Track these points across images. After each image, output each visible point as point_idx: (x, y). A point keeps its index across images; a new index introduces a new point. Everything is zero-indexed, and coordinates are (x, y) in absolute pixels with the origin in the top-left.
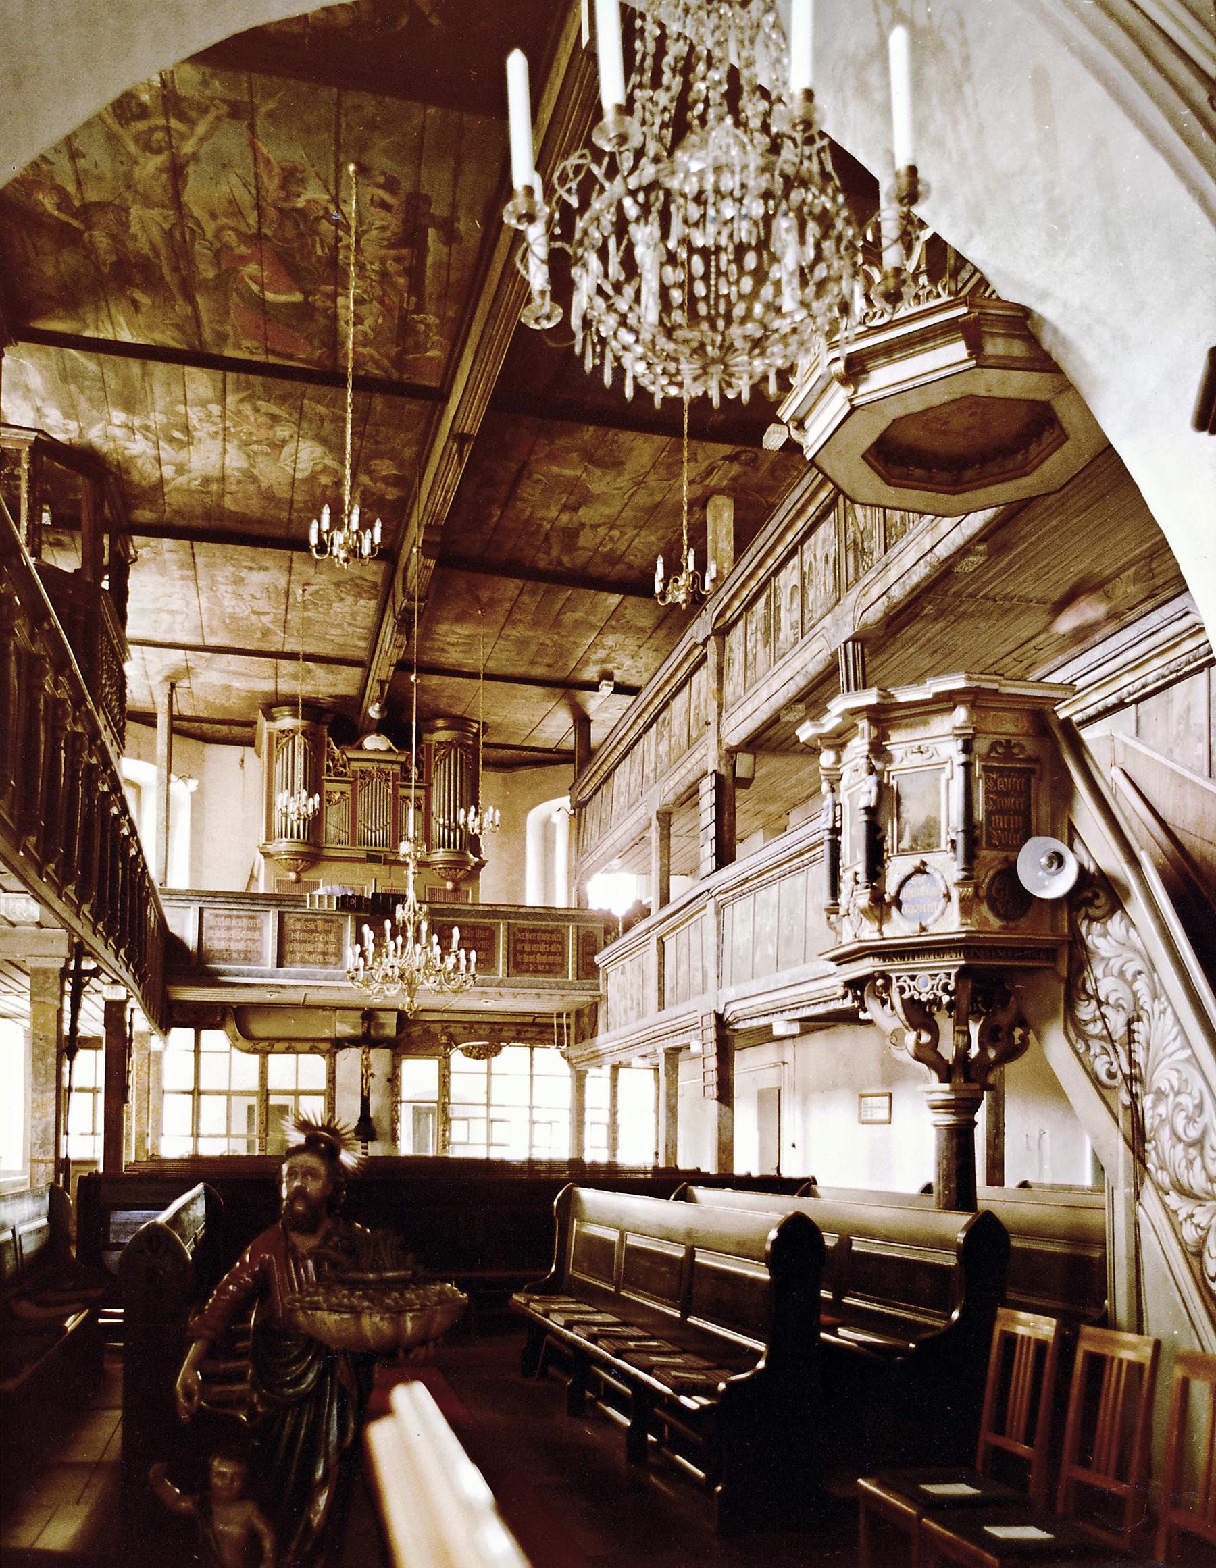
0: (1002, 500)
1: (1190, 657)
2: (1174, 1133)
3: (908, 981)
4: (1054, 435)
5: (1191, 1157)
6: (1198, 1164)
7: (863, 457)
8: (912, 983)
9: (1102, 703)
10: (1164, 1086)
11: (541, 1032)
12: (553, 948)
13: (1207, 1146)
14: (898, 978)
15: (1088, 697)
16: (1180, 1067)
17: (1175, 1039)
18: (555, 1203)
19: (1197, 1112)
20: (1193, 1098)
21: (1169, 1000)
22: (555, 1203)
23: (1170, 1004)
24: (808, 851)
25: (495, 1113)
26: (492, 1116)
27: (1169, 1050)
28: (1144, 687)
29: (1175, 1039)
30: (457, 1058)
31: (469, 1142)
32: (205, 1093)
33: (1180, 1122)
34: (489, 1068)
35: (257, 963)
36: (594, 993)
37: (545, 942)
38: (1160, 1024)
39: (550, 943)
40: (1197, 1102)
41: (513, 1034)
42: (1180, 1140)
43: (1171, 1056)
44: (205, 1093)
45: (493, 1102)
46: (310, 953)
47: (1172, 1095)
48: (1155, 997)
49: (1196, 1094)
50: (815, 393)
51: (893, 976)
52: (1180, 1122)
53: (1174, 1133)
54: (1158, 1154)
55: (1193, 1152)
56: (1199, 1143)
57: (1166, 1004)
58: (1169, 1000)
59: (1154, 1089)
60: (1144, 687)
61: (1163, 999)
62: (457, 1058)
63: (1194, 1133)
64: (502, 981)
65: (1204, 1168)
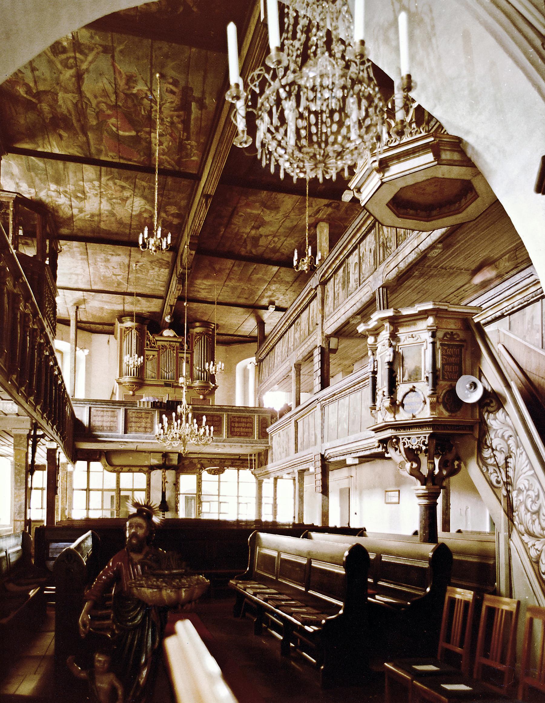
1: (534, 294)
2: (526, 508)
3: (407, 440)
5: (534, 519)
6: (537, 522)
8: (409, 441)
9: (494, 315)
10: (522, 487)
11: (243, 463)
12: (248, 425)
13: (541, 514)
14: (403, 439)
15: (488, 313)
16: (529, 478)
17: (527, 466)
18: (249, 539)
19: (537, 499)
20: (535, 492)
21: (524, 448)
22: (249, 539)
23: (525, 450)
24: (362, 382)
25: (222, 499)
26: (221, 501)
28: (513, 308)
29: (527, 466)
30: (205, 474)
31: (210, 512)
32: (92, 490)
33: (529, 503)
34: (219, 479)
35: (115, 432)
36: (266, 445)
37: (244, 422)
38: (520, 459)
42: (529, 511)
43: (525, 473)
44: (92, 490)
45: (221, 494)
46: (139, 427)
47: (525, 491)
48: (518, 447)
51: (400, 437)
52: (529, 503)
54: (519, 518)
55: (535, 516)
56: (537, 513)
57: (523, 450)
58: (524, 448)
59: (517, 488)
60: (513, 308)
61: (521, 448)
62: (205, 474)
63: (535, 508)
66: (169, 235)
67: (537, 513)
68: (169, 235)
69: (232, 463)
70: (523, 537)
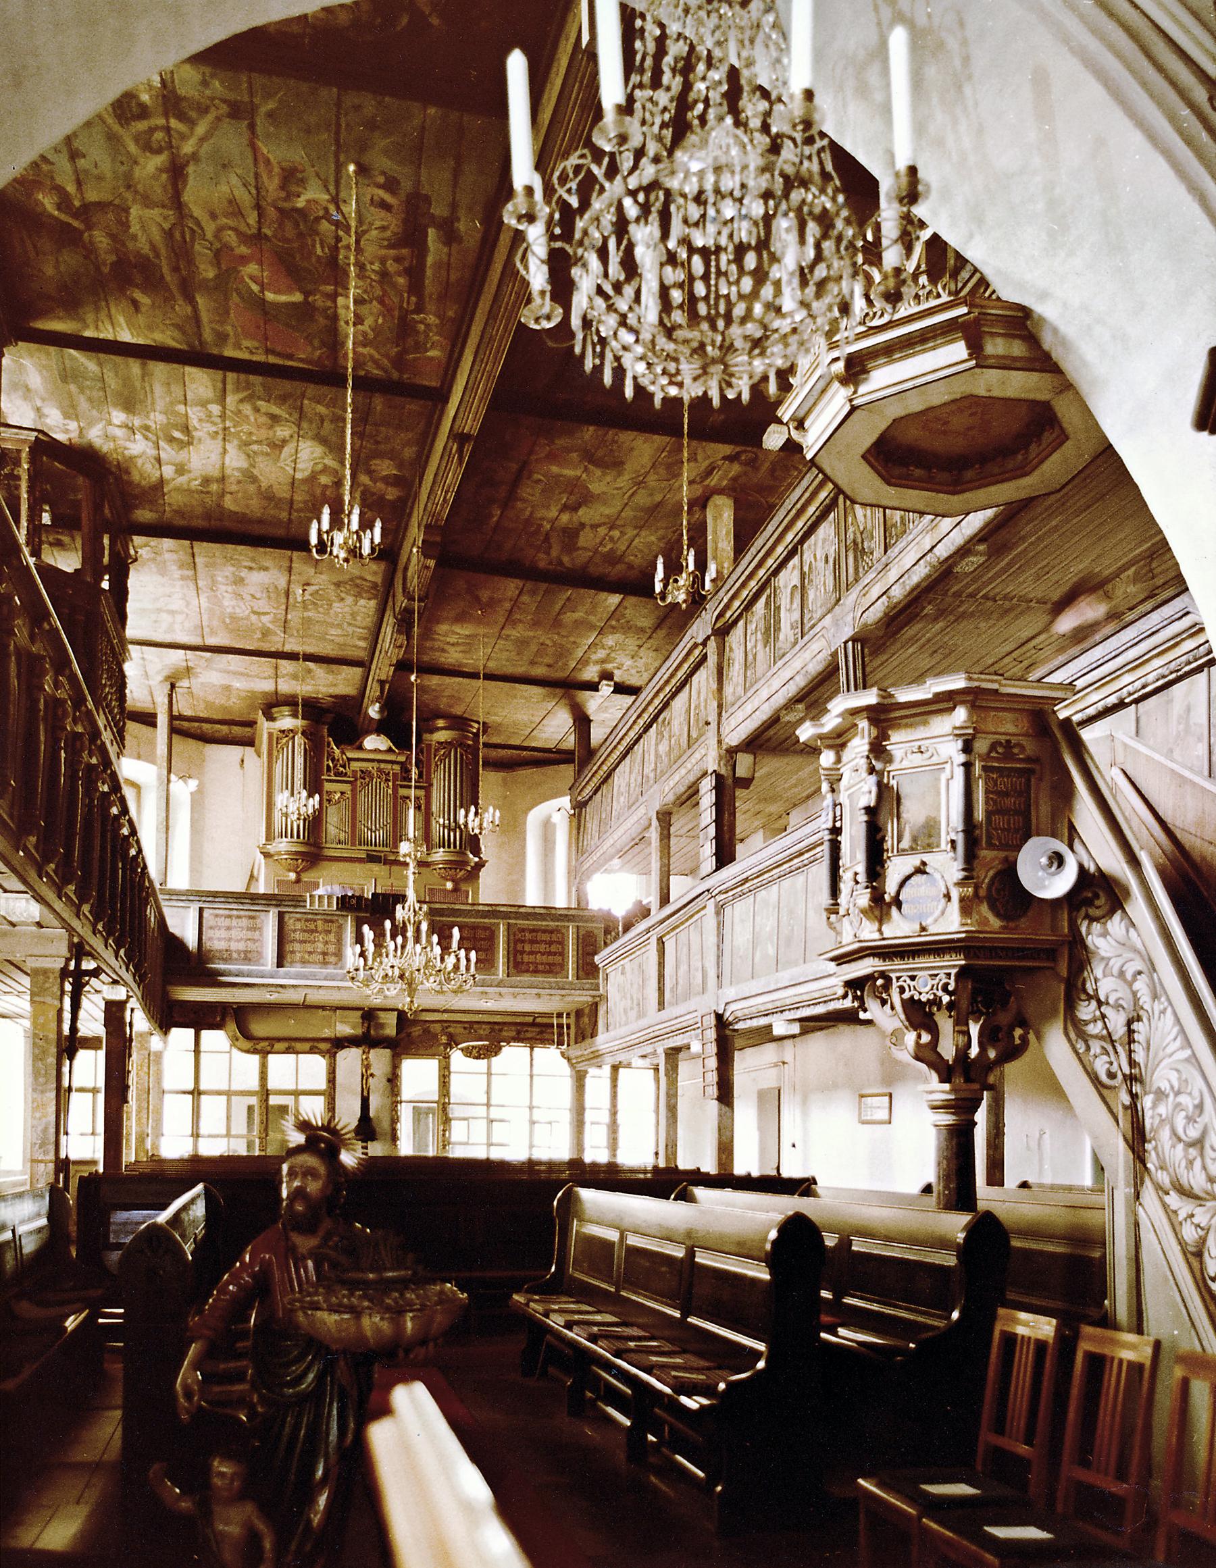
0: (1002, 500)
1: (1190, 657)
3: (908, 981)
4: (1054, 435)
5: (1191, 1157)
6: (1198, 1164)
7: (863, 457)
8: (912, 983)
9: (1102, 703)
10: (1164, 1086)
11: (541, 1032)
12: (553, 948)
13: (1207, 1146)
14: (898, 978)
15: (1088, 697)
16: (1180, 1067)
17: (1175, 1039)
18: (555, 1203)
19: (1197, 1112)
20: (1193, 1098)
21: (1169, 1000)
22: (555, 1203)
23: (1170, 1004)
24: (808, 851)
25: (495, 1113)
26: (492, 1116)
27: (1169, 1050)
28: (1144, 687)
29: (1175, 1039)
30: (457, 1058)
31: (469, 1142)
32: (205, 1093)
33: (1180, 1122)
34: (489, 1068)
36: (594, 993)
37: (545, 942)
39: (550, 943)
40: (1197, 1102)
41: (513, 1034)
42: (1180, 1140)
44: (205, 1093)
45: (493, 1102)
47: (1172, 1095)
48: (1155, 997)
49: (1196, 1094)
50: (815, 393)
51: (893, 976)
52: (1180, 1122)
53: (1174, 1133)
54: (1158, 1154)
55: (1193, 1152)
56: (1199, 1143)
57: (1166, 1004)
58: (1169, 1000)
59: (1154, 1089)
60: (1144, 687)
61: (1163, 999)
62: (457, 1058)
63: (1194, 1133)
64: (502, 981)
65: (1204, 1168)
66: (378, 525)
67: (1199, 1143)
68: (378, 525)
69: (519, 1032)
70: (1167, 1199)
